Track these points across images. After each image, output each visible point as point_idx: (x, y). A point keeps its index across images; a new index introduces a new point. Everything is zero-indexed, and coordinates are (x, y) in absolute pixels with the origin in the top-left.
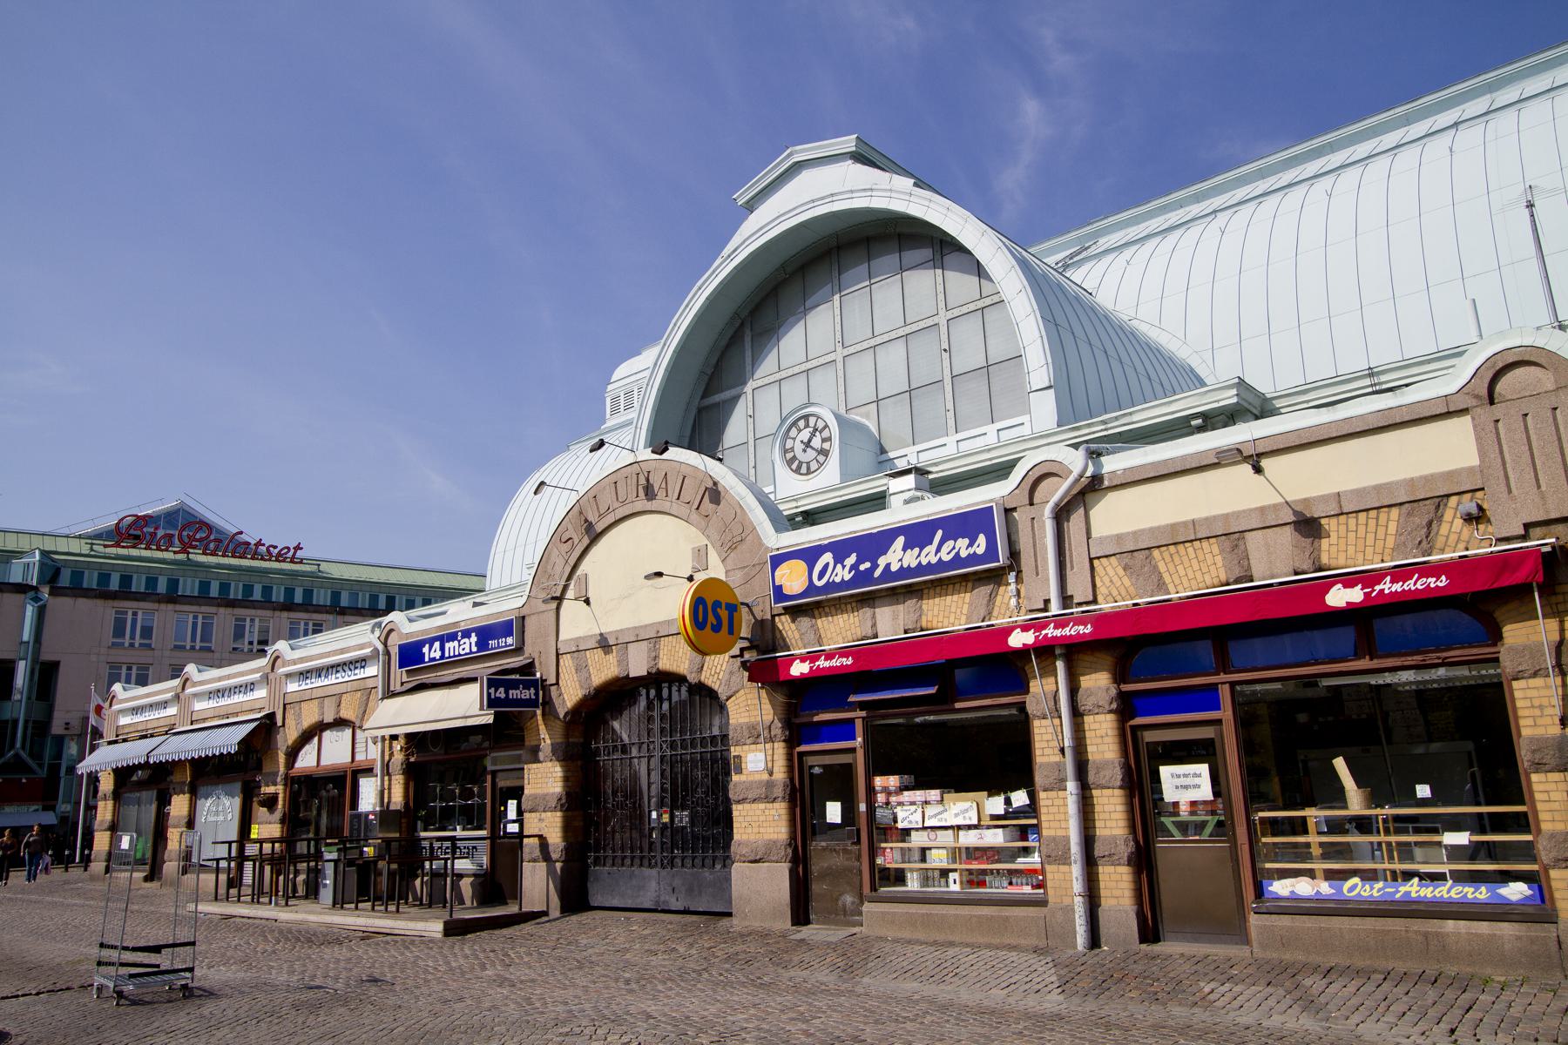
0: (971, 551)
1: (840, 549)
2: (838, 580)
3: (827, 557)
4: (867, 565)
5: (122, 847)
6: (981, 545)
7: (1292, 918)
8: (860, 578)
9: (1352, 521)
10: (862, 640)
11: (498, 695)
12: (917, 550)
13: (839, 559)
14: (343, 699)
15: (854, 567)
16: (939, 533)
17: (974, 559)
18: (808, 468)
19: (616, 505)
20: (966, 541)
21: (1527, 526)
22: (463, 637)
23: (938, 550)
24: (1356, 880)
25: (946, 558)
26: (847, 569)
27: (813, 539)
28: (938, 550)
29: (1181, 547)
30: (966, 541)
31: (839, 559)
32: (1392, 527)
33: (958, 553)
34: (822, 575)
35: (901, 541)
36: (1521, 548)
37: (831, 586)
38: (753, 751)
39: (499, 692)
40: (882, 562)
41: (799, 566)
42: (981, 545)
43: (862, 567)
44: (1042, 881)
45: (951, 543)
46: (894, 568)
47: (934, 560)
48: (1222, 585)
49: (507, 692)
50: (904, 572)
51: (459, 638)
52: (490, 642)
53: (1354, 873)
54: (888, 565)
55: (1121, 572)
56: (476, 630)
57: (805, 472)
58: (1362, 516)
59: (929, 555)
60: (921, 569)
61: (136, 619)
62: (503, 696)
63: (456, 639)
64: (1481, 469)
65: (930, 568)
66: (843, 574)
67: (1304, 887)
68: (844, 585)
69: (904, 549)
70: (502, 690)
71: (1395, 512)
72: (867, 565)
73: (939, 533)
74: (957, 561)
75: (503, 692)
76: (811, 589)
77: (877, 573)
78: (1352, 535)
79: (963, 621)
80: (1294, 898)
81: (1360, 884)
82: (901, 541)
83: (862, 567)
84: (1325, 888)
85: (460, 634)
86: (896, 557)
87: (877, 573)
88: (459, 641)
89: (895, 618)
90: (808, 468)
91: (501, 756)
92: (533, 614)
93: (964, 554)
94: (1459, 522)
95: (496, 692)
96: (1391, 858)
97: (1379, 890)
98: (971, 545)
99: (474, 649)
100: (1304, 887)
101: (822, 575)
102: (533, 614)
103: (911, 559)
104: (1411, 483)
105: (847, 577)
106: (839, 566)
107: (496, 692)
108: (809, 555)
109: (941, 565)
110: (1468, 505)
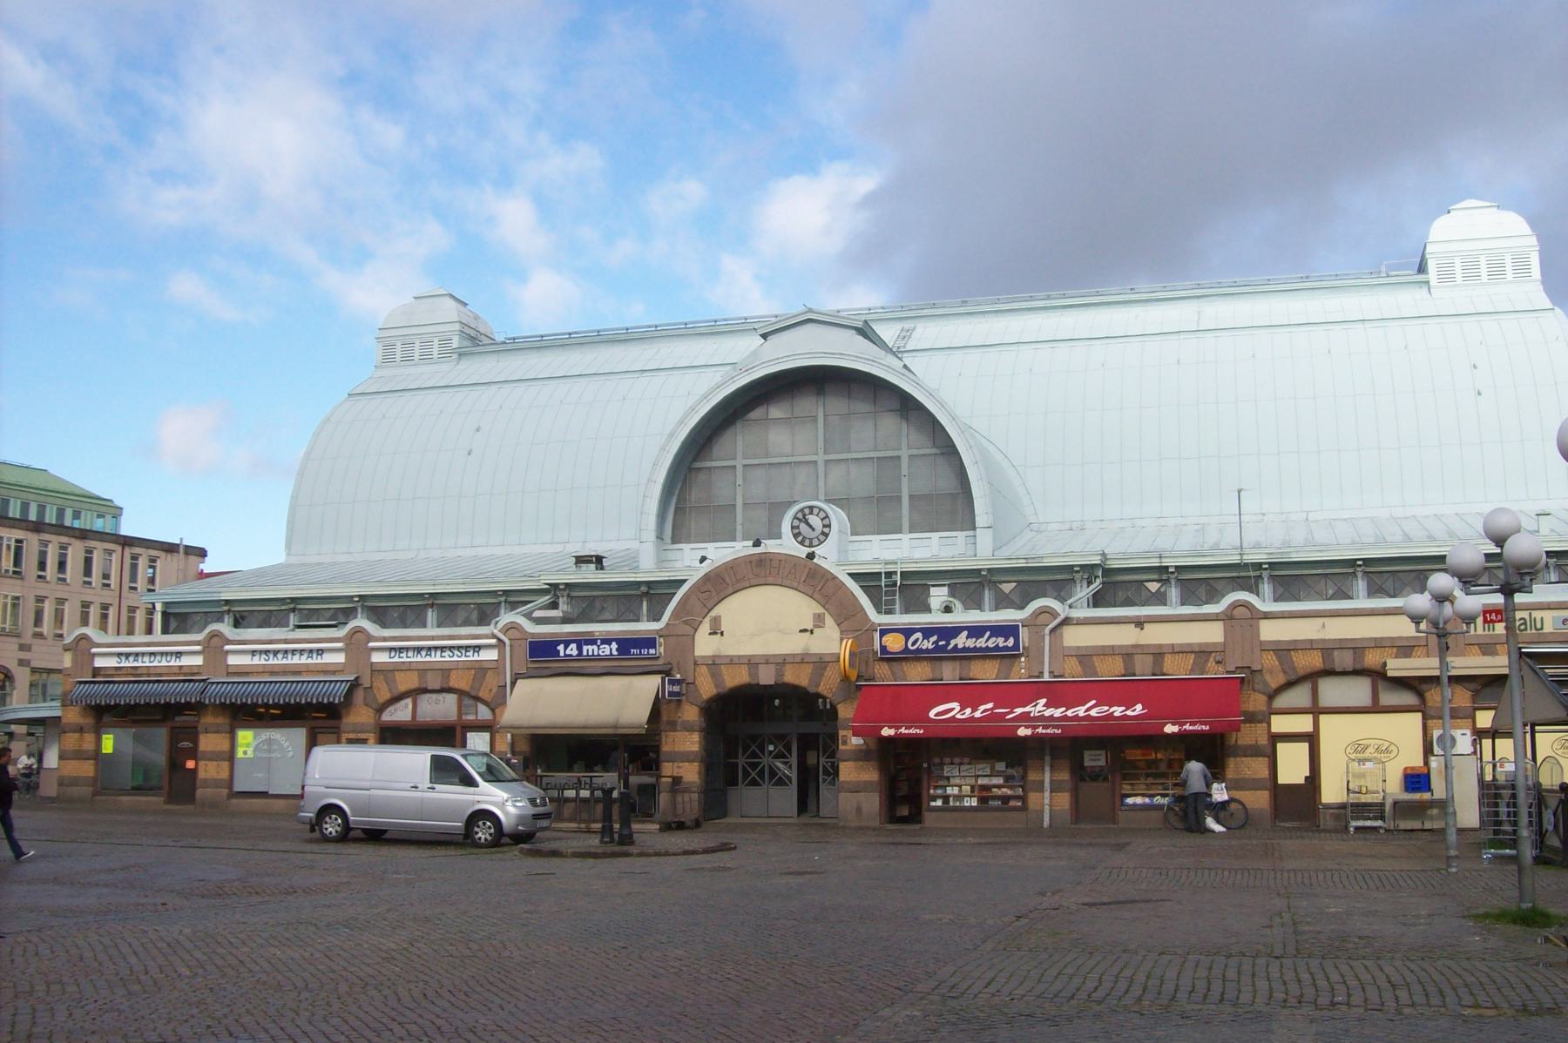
0: (1005, 644)
1: (927, 632)
2: (924, 647)
3: (919, 635)
4: (943, 643)
6: (1011, 642)
7: (635, 569)
8: (937, 649)
9: (1177, 656)
10: (932, 680)
11: (568, 652)
12: (974, 640)
14: (452, 674)
15: (935, 643)
16: (988, 633)
17: (1006, 648)
18: (811, 543)
19: (751, 576)
20: (1003, 639)
21: (1237, 668)
22: (602, 644)
23: (987, 641)
24: (1159, 797)
25: (991, 646)
26: (931, 643)
27: (904, 621)
28: (987, 641)
29: (1106, 657)
30: (1003, 639)
32: (1191, 661)
33: (998, 645)
34: (914, 644)
35: (965, 633)
37: (919, 650)
38: (767, 660)
39: (570, 648)
40: (953, 643)
41: (901, 637)
42: (1011, 642)
43: (940, 643)
45: (994, 639)
46: (960, 646)
47: (984, 646)
48: (1123, 676)
49: (580, 649)
50: (965, 649)
51: (599, 644)
52: (632, 650)
53: (1158, 795)
54: (956, 645)
55: (1078, 664)
56: (618, 641)
57: (808, 544)
58: (1181, 655)
59: (981, 643)
60: (975, 649)
61: (136, 564)
62: (575, 652)
63: (596, 644)
64: (1225, 644)
65: (981, 649)
66: (928, 645)
67: (1139, 800)
68: (927, 651)
69: (967, 638)
70: (573, 646)
71: (1193, 656)
72: (943, 643)
73: (988, 633)
74: (997, 648)
75: (575, 648)
76: (906, 650)
77: (950, 647)
78: (1176, 662)
79: (994, 677)
80: (1135, 805)
82: (965, 633)
83: (940, 643)
84: (1147, 800)
85: (599, 641)
86: (961, 641)
87: (950, 647)
88: (599, 646)
89: (954, 669)
90: (811, 543)
92: (672, 636)
93: (1001, 645)
94: (1214, 663)
95: (566, 649)
98: (1005, 641)
99: (615, 653)
100: (1139, 800)
101: (914, 644)
102: (672, 636)
103: (971, 643)
104: (1200, 644)
105: (930, 647)
106: (926, 641)
107: (566, 649)
108: (907, 632)
110: (1219, 658)
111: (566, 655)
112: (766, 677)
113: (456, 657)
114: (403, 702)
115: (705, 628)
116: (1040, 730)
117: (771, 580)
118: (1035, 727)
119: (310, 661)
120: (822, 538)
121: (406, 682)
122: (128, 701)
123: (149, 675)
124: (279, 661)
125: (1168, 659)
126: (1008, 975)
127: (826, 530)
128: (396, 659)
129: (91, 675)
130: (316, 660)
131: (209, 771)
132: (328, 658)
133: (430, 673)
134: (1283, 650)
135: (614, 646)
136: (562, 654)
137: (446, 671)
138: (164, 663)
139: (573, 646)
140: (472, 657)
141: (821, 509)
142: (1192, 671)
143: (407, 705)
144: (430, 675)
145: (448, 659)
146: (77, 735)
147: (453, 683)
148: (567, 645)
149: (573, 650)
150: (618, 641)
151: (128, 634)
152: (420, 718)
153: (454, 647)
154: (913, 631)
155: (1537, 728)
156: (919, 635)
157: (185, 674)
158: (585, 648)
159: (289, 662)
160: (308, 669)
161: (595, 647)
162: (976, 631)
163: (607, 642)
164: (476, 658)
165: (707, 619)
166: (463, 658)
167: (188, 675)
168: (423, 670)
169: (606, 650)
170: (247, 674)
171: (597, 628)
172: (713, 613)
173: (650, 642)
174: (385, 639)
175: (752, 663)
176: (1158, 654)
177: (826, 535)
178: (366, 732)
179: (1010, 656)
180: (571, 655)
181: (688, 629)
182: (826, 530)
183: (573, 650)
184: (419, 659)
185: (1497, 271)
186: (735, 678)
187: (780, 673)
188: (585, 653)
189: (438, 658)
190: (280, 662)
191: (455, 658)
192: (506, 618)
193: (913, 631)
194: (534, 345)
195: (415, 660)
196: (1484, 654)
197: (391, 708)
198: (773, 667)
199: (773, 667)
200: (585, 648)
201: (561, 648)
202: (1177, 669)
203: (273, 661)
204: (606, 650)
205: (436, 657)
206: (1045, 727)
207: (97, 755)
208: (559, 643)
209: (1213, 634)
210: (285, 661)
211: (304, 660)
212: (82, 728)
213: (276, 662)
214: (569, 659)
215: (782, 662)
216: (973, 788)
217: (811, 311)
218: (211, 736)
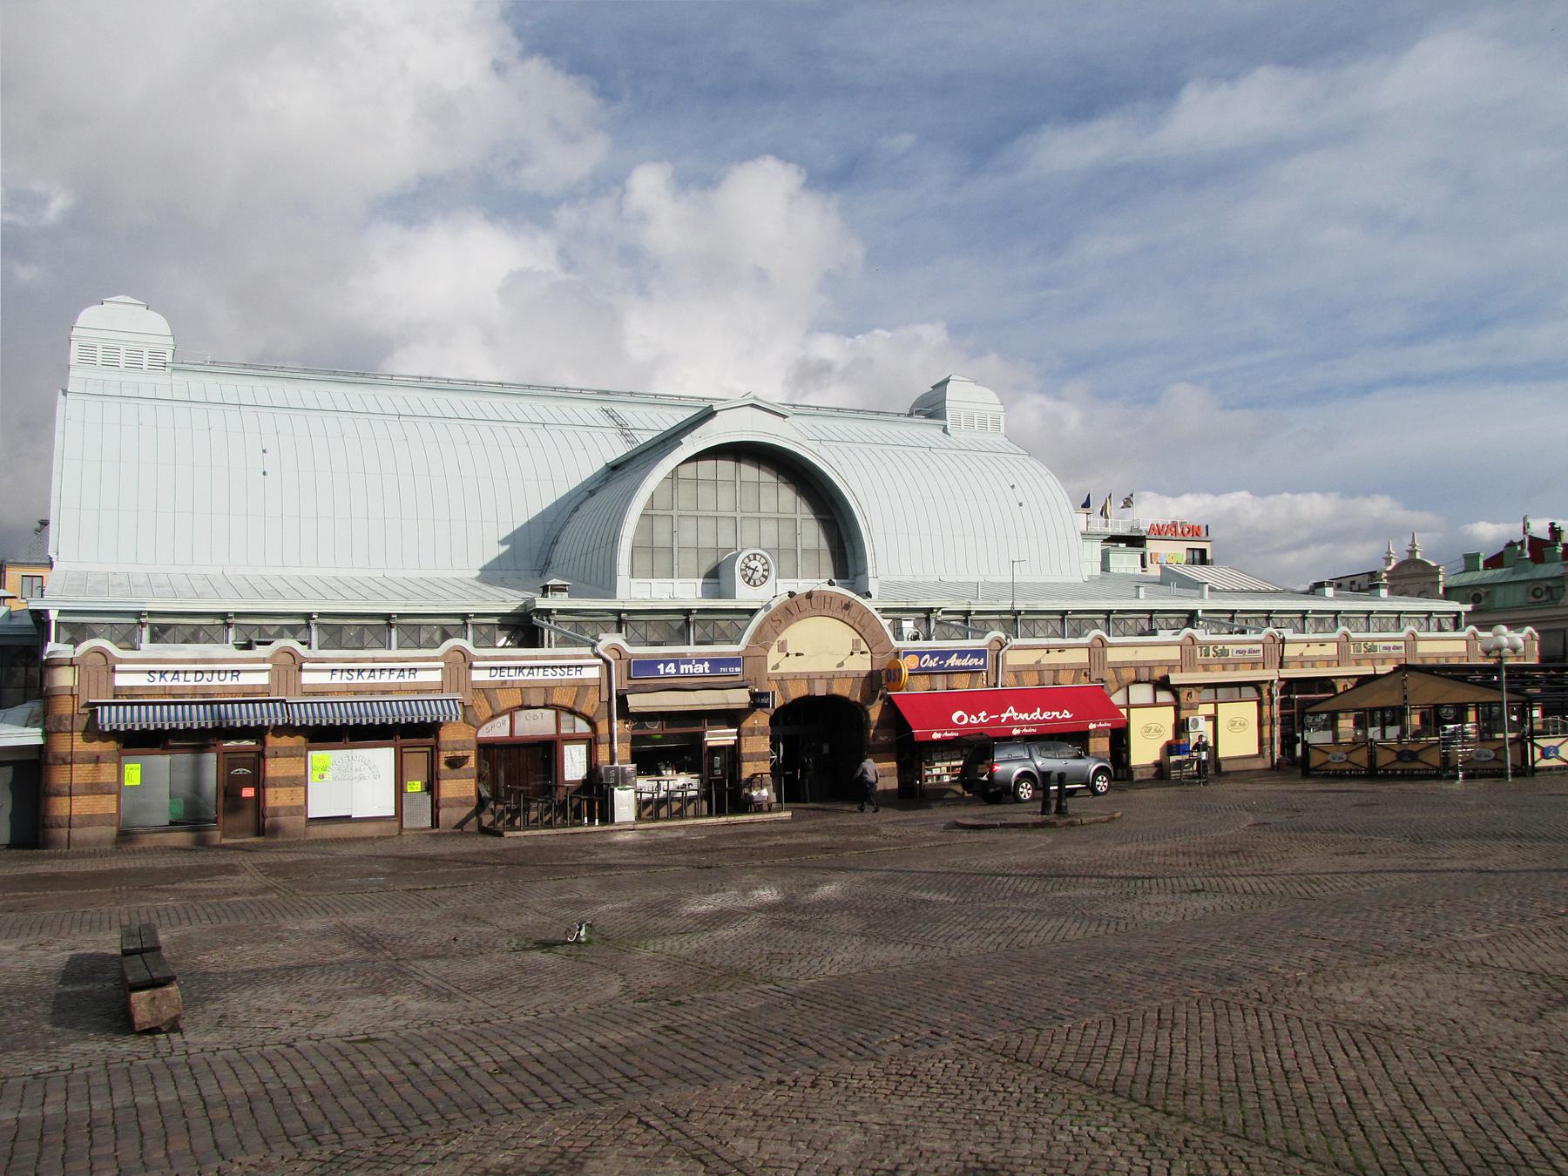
1: (933, 654)
3: (927, 656)
5: (39, 741)
11: (667, 671)
13: (932, 658)
15: (937, 662)
31: (932, 658)
35: (956, 655)
36: (751, 823)
37: (927, 668)
38: (821, 676)
40: (948, 662)
41: (916, 658)
44: (1168, 777)
49: (677, 668)
50: (955, 667)
56: (710, 661)
59: (965, 662)
60: (961, 667)
62: (673, 671)
65: (964, 667)
66: (932, 664)
68: (932, 668)
70: (672, 665)
74: (973, 666)
81: (966, 716)
82: (956, 655)
86: (953, 661)
91: (1512, 760)
96: (591, 821)
97: (985, 718)
103: (959, 663)
108: (920, 654)
109: (968, 667)
111: (665, 673)
112: (820, 690)
113: (559, 675)
114: (500, 719)
115: (774, 648)
116: (1025, 730)
117: (824, 613)
118: (1022, 728)
119: (401, 680)
120: (763, 579)
121: (509, 699)
122: (397, 720)
123: (194, 695)
124: (365, 679)
125: (1061, 673)
126: (1376, 875)
127: (766, 573)
128: (497, 678)
129: (111, 694)
130: (408, 679)
131: (276, 798)
132: (422, 677)
133: (532, 690)
134: (1117, 668)
135: (707, 665)
136: (662, 672)
137: (547, 689)
138: (216, 682)
139: (672, 665)
140: (574, 675)
141: (762, 556)
142: (1073, 682)
143: (504, 723)
144: (532, 693)
145: (550, 677)
146: (90, 767)
147: (556, 700)
148: (666, 663)
149: (671, 669)
150: (710, 661)
151: (925, 639)
152: (517, 733)
153: (556, 667)
154: (925, 653)
155: (404, 750)
156: (927, 656)
157: (174, 696)
158: (682, 667)
159: (377, 680)
160: (400, 689)
161: (691, 666)
162: (962, 654)
163: (701, 661)
164: (578, 676)
165: (776, 643)
166: (566, 677)
167: (250, 697)
168: (524, 689)
169: (699, 669)
170: (323, 693)
171: (691, 649)
172: (781, 638)
173: (734, 662)
174: (486, 659)
175: (810, 679)
176: (1056, 670)
177: (766, 577)
178: (469, 749)
179: (973, 672)
180: (670, 673)
181: (762, 652)
182: (766, 573)
183: (671, 669)
184: (521, 677)
185: (983, 425)
186: (797, 691)
187: (829, 686)
188: (682, 672)
189: (541, 676)
190: (366, 681)
191: (558, 677)
192: (279, 644)
193: (925, 653)
194: (411, 384)
195: (517, 678)
196: (1205, 670)
197: (488, 725)
198: (824, 681)
199: (824, 681)
200: (682, 667)
201: (661, 667)
202: (1066, 681)
203: (356, 679)
204: (699, 669)
205: (539, 675)
206: (1028, 728)
207: (117, 789)
208: (659, 662)
209: (1081, 657)
210: (371, 680)
211: (394, 678)
212: (98, 757)
213: (361, 680)
214: (668, 676)
215: (830, 678)
216: (948, 768)
217: (755, 398)
218: (282, 761)
